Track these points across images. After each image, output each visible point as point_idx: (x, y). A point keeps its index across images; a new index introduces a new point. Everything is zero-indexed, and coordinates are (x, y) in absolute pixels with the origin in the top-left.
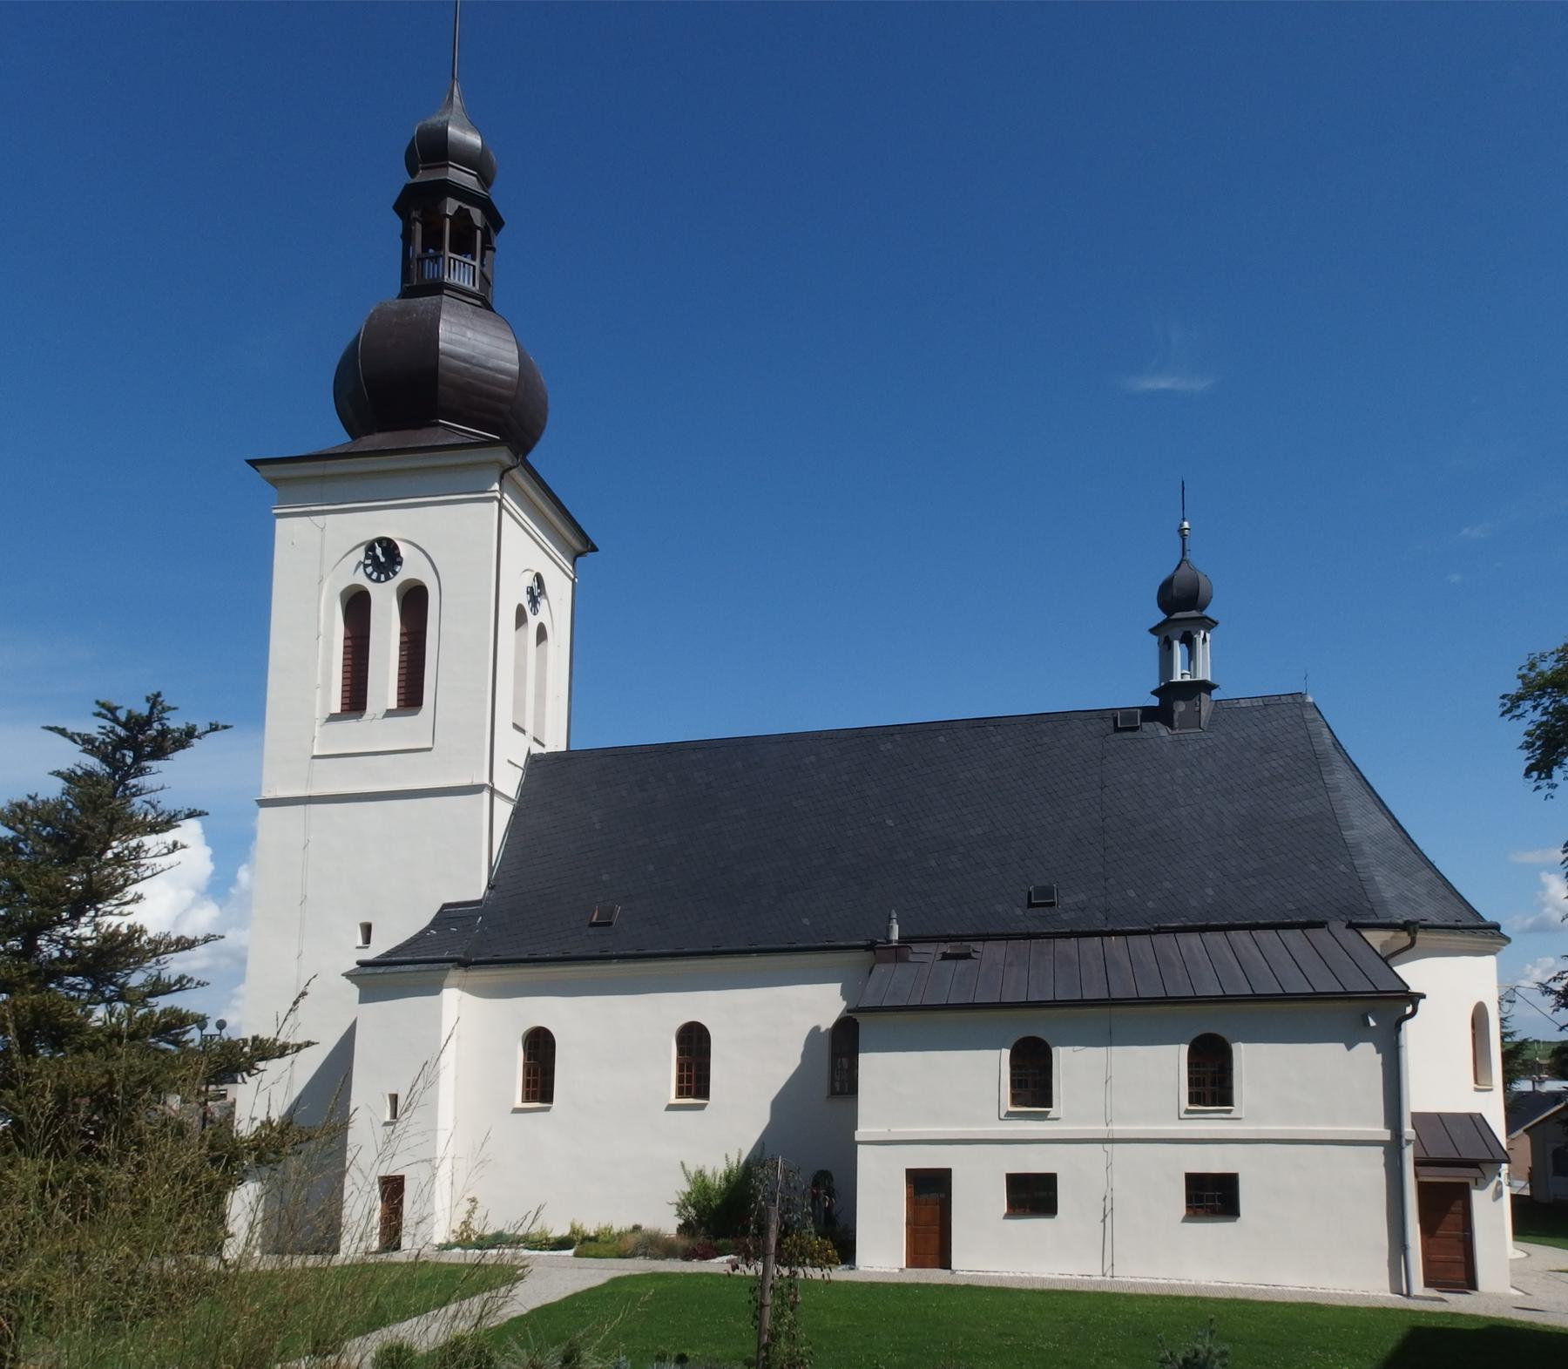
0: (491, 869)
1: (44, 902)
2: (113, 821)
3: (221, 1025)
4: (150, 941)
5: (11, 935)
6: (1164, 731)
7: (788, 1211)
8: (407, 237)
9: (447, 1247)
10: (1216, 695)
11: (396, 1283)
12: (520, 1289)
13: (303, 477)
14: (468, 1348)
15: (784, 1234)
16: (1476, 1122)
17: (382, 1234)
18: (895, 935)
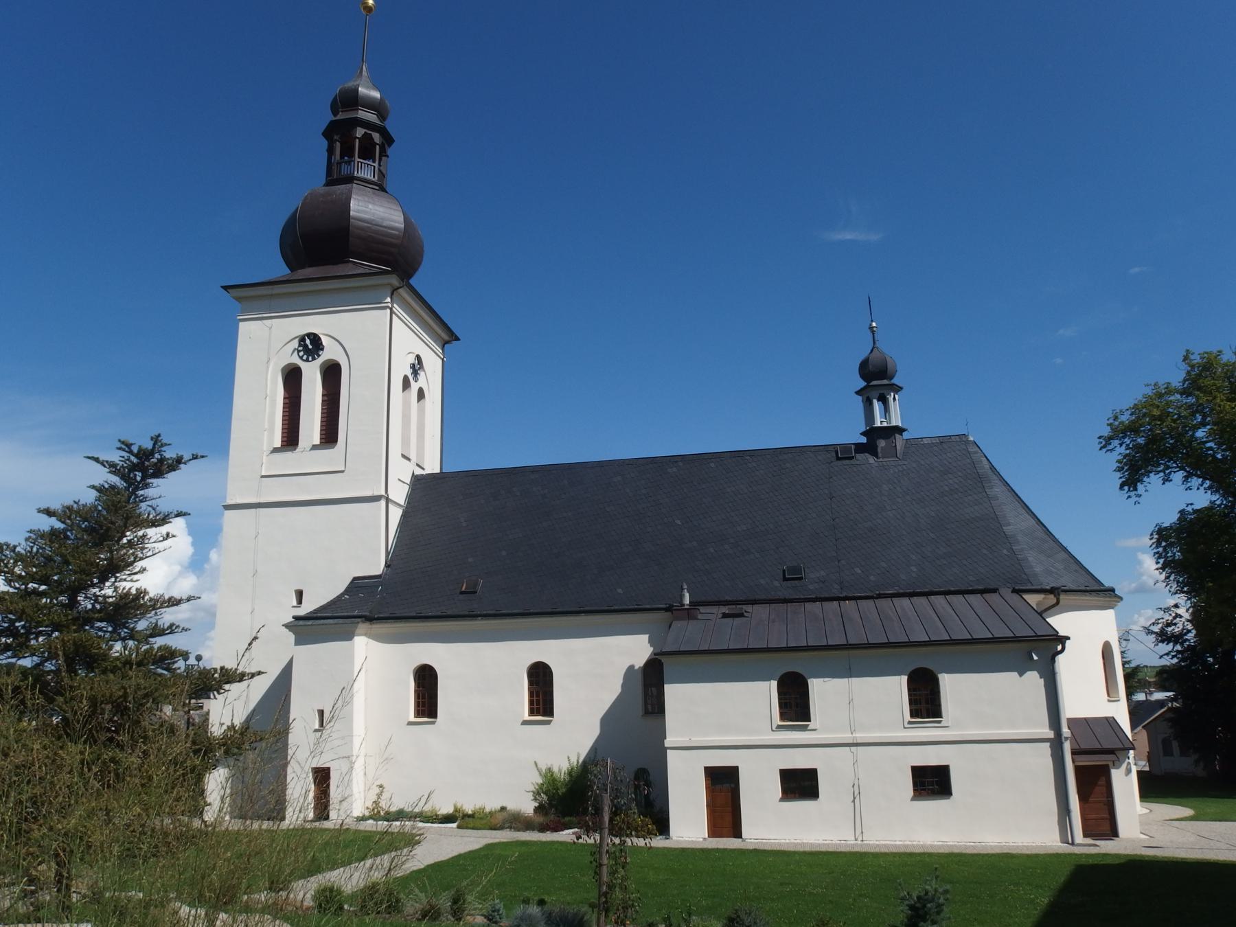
0: (387, 553)
1: (82, 572)
2: (127, 518)
3: (199, 658)
4: (151, 599)
5: (61, 593)
6: (871, 460)
7: (617, 797)
8: (330, 151)
9: (363, 819)
10: (906, 435)
11: (327, 844)
12: (418, 850)
13: (258, 296)
14: (382, 891)
15: (615, 812)
16: (1111, 722)
17: (315, 808)
18: (687, 601)
